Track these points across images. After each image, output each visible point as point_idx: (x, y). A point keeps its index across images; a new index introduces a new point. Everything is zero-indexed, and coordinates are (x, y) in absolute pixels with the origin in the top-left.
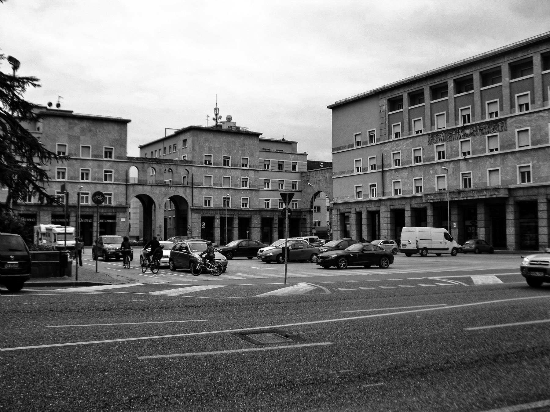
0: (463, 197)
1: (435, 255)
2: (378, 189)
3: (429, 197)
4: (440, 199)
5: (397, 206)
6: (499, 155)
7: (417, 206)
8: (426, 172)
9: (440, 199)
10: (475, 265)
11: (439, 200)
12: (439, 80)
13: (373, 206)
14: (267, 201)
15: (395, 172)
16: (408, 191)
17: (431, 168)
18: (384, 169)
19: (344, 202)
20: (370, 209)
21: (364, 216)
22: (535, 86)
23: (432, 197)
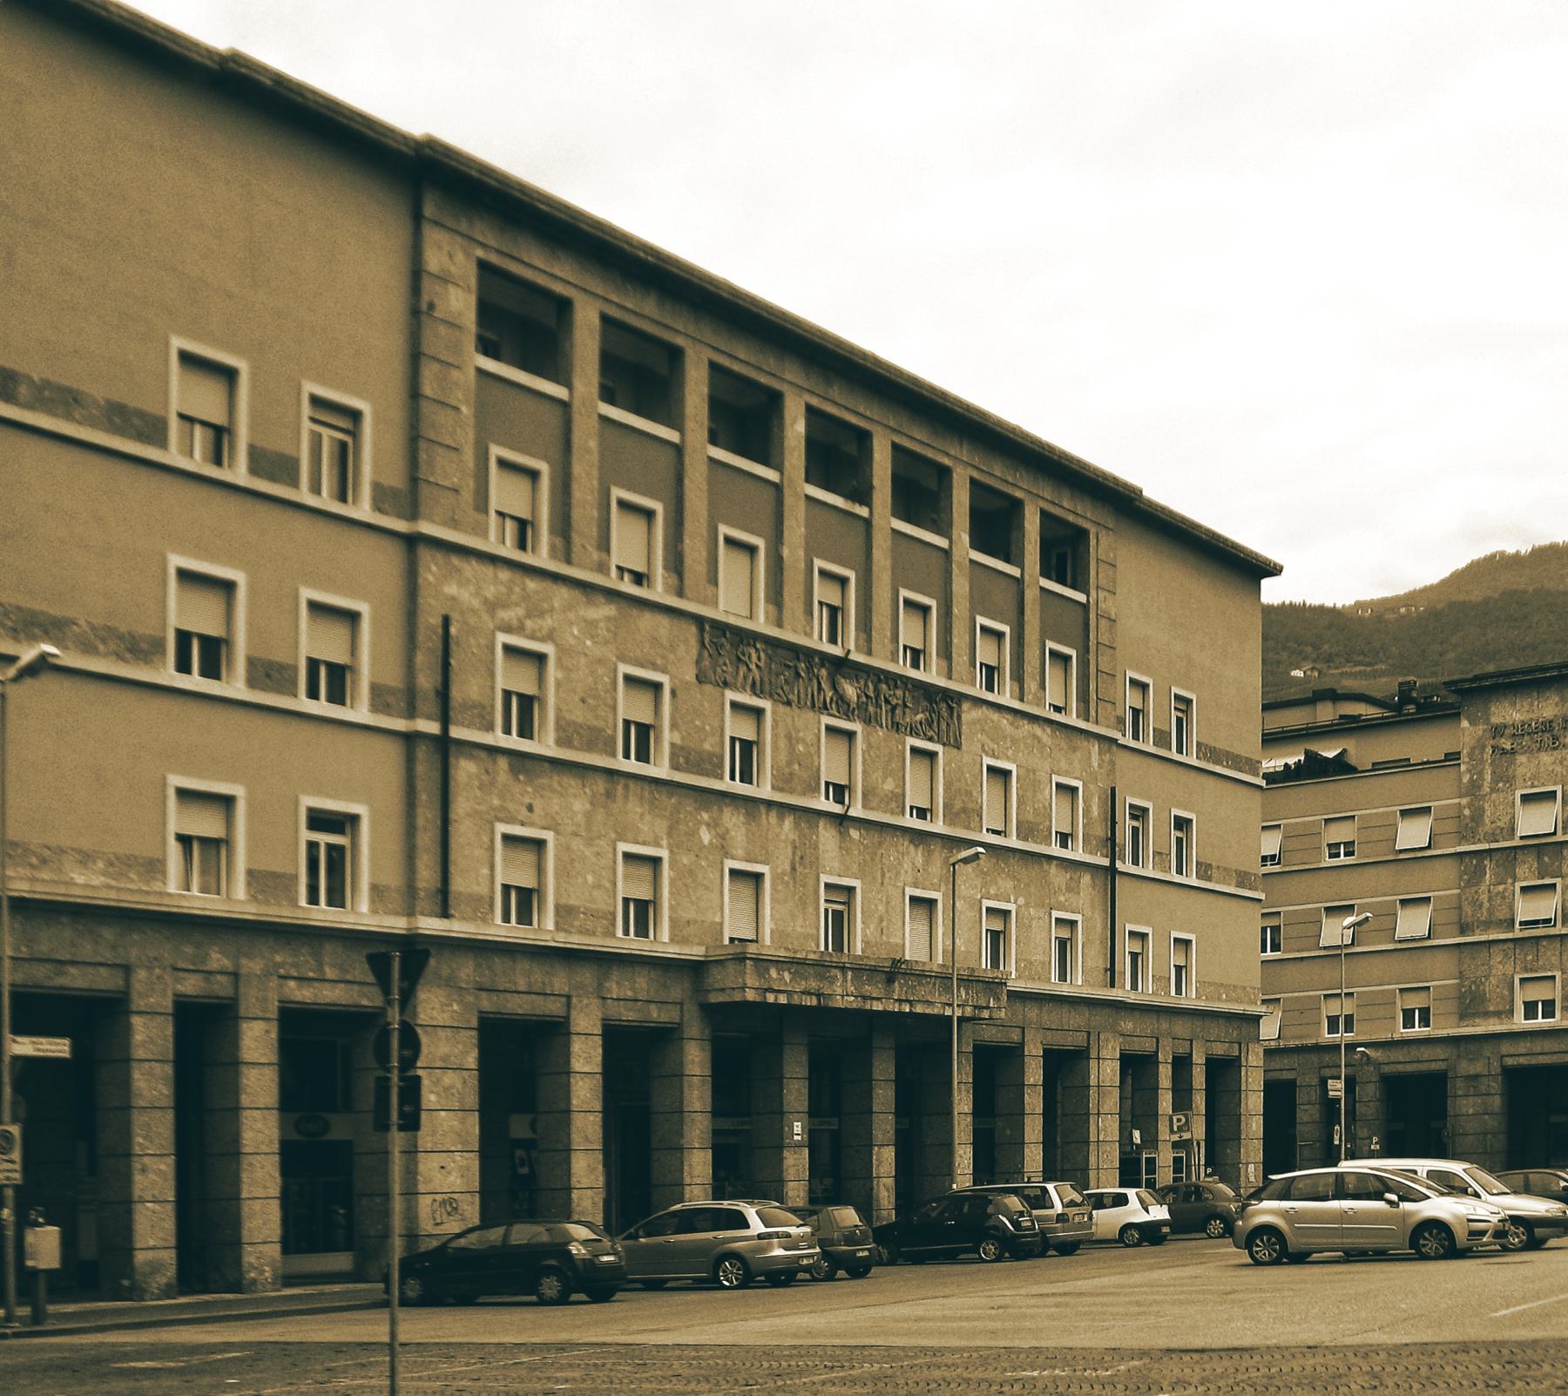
0: (900, 1001)
1: (1498, 1247)
3: (773, 973)
4: (819, 996)
6: (1018, 856)
8: (682, 827)
9: (819, 996)
11: (814, 1002)
12: (752, 360)
13: (330, 973)
14: (323, 838)
16: (593, 914)
17: (705, 816)
19: (57, 893)
22: (574, 501)
23: (787, 976)
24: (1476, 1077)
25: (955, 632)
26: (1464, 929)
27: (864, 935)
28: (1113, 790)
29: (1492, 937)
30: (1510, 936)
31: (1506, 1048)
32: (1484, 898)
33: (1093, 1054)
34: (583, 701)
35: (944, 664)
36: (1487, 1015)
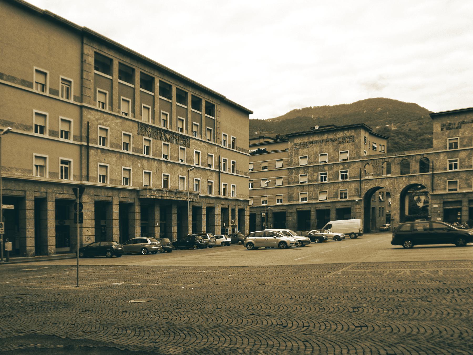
0: (178, 198)
2: (73, 169)
3: (153, 192)
4: (162, 197)
5: (103, 197)
7: (125, 201)
10: (455, 251)
11: (161, 198)
12: (148, 71)
13: (65, 192)
15: (102, 152)
18: (434, 172)
20: (60, 196)
21: (51, 206)
24: (292, 213)
25: (189, 125)
26: (289, 184)
27: (171, 185)
28: (220, 156)
30: (298, 185)
32: (293, 177)
34: (115, 138)
35: (186, 131)
36: (294, 200)
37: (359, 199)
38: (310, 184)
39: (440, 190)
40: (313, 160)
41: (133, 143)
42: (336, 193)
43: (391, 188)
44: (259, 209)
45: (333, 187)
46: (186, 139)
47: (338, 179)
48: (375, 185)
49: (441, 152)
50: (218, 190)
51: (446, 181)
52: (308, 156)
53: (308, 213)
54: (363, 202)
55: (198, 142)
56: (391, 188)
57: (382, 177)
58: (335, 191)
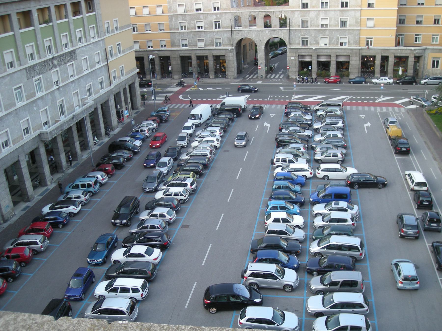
4: (61, 130)
24: (175, 58)
25: (72, 37)
26: (170, 30)
27: (66, 106)
28: (106, 49)
29: (175, 31)
30: (178, 31)
31: (180, 52)
32: (173, 24)
33: (109, 100)
34: (8, 99)
35: (71, 44)
36: (176, 46)
37: (231, 48)
38: (189, 31)
39: (296, 44)
40: (189, 8)
41: (25, 92)
42: (212, 42)
43: (257, 39)
44: (146, 52)
45: (208, 35)
46: (72, 55)
47: (212, 28)
48: (244, 35)
49: (295, 11)
50: (105, 57)
51: (300, 37)
52: (184, 4)
53: (189, 58)
54: (235, 51)
55: (84, 49)
56: (257, 39)
57: (249, 29)
58: (210, 39)
